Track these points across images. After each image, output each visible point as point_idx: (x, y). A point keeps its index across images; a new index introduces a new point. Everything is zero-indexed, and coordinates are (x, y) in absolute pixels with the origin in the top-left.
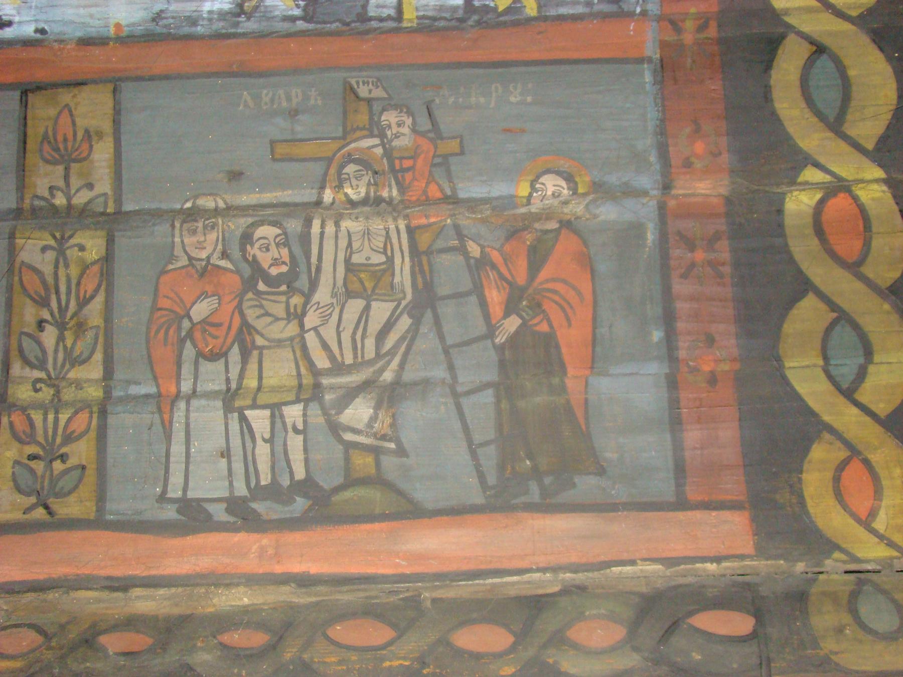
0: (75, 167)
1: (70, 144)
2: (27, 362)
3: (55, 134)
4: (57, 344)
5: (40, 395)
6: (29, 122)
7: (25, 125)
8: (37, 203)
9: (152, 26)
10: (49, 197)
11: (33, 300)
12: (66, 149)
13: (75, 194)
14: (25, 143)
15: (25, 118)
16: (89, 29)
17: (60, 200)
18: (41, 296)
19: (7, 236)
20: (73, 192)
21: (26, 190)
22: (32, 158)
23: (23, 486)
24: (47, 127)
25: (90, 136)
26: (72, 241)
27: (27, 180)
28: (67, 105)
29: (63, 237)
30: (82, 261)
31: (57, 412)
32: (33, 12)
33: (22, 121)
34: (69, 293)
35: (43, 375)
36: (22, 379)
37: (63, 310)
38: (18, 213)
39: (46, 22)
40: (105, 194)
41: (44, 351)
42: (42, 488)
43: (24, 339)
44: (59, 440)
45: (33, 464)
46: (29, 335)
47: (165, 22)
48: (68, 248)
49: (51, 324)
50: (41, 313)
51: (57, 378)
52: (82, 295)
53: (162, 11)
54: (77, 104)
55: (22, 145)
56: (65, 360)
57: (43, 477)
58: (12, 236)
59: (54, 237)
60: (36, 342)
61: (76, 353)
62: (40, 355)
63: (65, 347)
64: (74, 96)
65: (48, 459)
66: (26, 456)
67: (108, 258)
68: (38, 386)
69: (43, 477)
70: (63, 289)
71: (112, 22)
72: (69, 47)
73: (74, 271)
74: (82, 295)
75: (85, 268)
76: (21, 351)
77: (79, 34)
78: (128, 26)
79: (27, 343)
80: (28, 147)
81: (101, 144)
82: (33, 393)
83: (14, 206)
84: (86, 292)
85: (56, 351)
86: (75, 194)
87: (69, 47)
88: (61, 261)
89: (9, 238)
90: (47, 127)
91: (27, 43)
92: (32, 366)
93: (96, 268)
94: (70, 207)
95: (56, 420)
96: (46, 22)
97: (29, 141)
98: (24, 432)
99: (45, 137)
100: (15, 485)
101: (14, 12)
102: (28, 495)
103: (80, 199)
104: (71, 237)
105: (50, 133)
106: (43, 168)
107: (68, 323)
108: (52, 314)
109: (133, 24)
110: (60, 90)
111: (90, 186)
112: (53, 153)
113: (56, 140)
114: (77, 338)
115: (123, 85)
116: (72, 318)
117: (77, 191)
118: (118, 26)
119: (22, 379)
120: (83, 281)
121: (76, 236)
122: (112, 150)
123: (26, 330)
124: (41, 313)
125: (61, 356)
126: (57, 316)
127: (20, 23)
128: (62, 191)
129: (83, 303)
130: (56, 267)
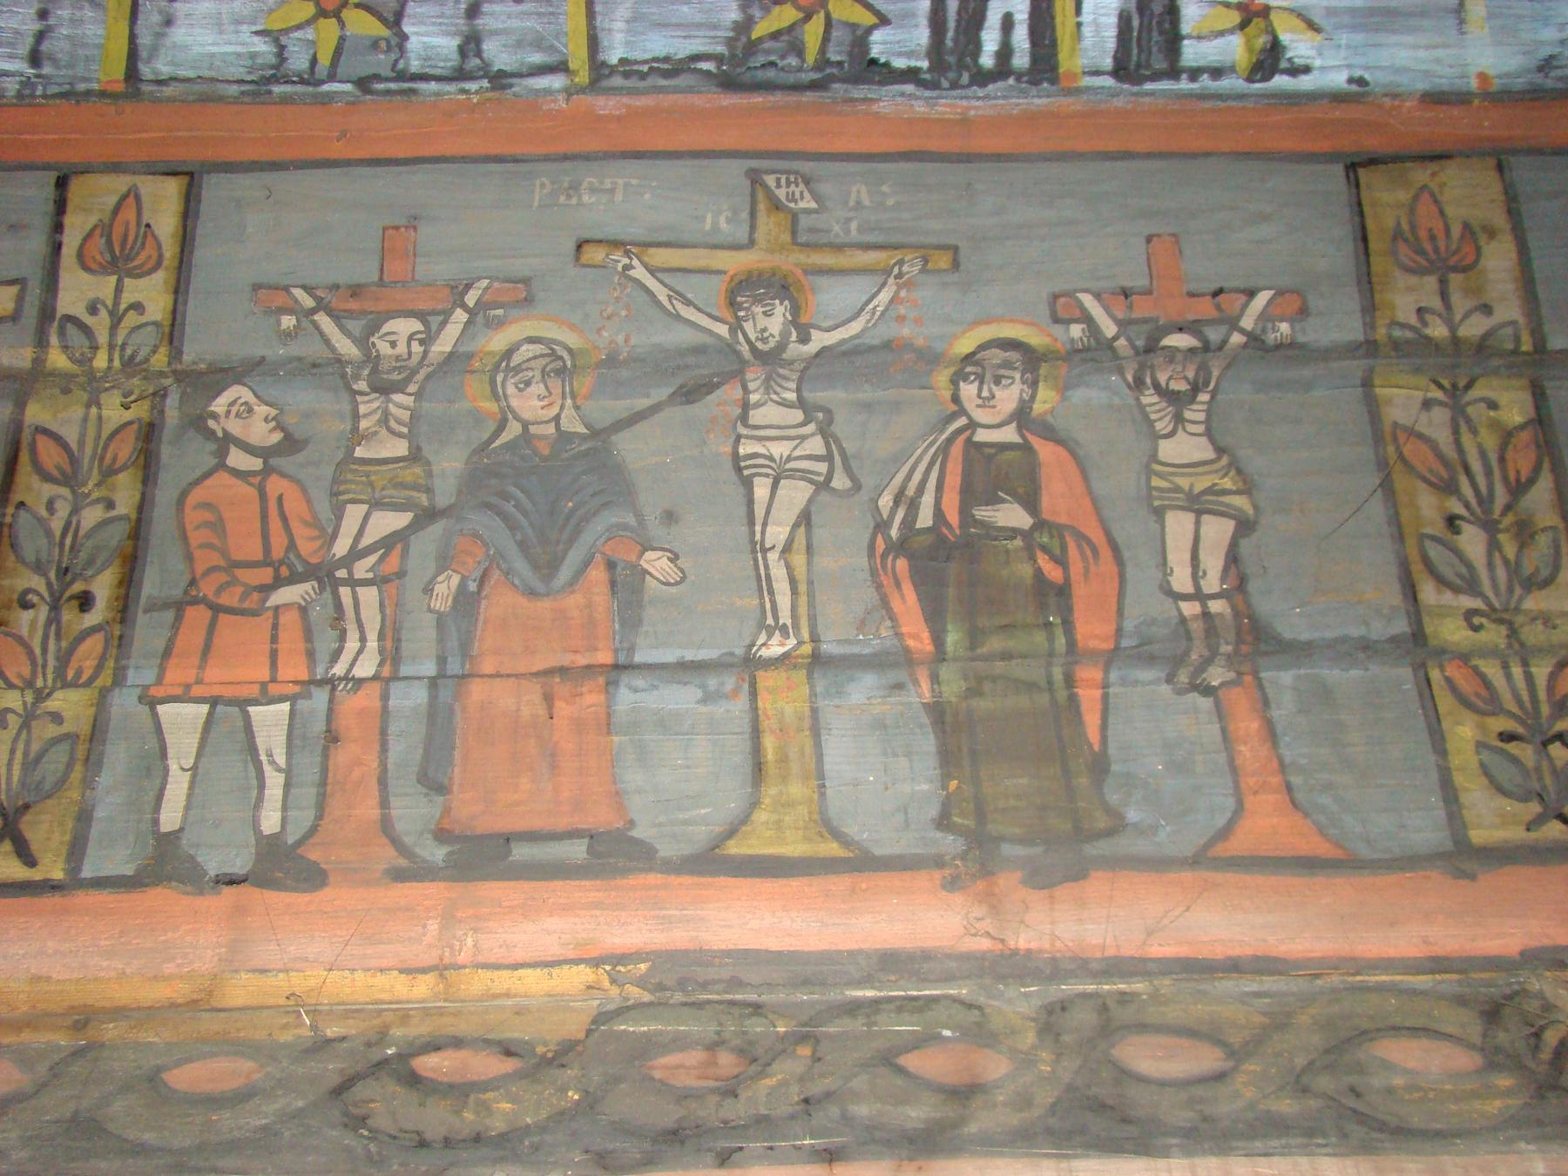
0: (1455, 279)
1: (1442, 244)
2: (1442, 582)
3: (1413, 227)
4: (1490, 555)
5: (1482, 636)
6: (1366, 209)
7: (1361, 214)
8: (1397, 333)
9: (1538, 79)
10: (1418, 325)
11: (1430, 484)
12: (1436, 250)
13: (1462, 320)
14: (1365, 239)
15: (1360, 204)
16: (1437, 80)
17: (1438, 331)
18: (1442, 479)
19: (1358, 382)
20: (1458, 317)
21: (1378, 313)
22: (1378, 263)
23: (1507, 786)
24: (1398, 218)
25: (1473, 233)
26: (1477, 392)
27: (1377, 297)
28: (1424, 188)
29: (1454, 386)
30: (1495, 425)
31: (1525, 664)
32: (1343, 53)
33: (1356, 209)
34: (1488, 473)
35: (1477, 604)
36: (1443, 612)
37: (1485, 501)
38: (1370, 348)
39: (1367, 68)
40: (1513, 323)
41: (1469, 565)
42: (1544, 787)
43: (1428, 543)
44: (1545, 710)
45: (1512, 748)
46: (1433, 538)
47: (1559, 72)
48: (1468, 404)
49: (1469, 522)
50: (1447, 504)
51: (1506, 610)
52: (1512, 476)
53: (1552, 57)
54: (1442, 185)
55: (1361, 244)
56: (1510, 581)
57: (1538, 769)
58: (1367, 384)
59: (1440, 386)
60: (1451, 550)
61: (1527, 569)
62: (1464, 570)
63: (1506, 562)
64: (1433, 175)
65: (1538, 739)
66: (1494, 735)
67: (1541, 420)
68: (1476, 620)
69: (1538, 769)
70: (1476, 466)
71: (1473, 70)
72: (1408, 104)
73: (1490, 441)
74: (1512, 476)
75: (1507, 436)
76: (1426, 561)
77: (1421, 86)
78: (1499, 77)
79: (1434, 551)
80: (1372, 245)
81: (1494, 244)
82: (1470, 633)
83: (1359, 336)
84: (1518, 472)
85: (1490, 565)
86: (1462, 320)
87: (1408, 104)
88: (1462, 423)
89: (1363, 385)
90: (1398, 218)
91: (1337, 98)
92: (1457, 590)
93: (1525, 436)
94: (1455, 341)
95: (1529, 678)
96: (1367, 68)
97: (1371, 237)
98: (1477, 695)
99: (1397, 235)
100: (1491, 782)
101: (1313, 53)
102: (1525, 800)
103: (1473, 328)
104: (1469, 386)
105: (1405, 226)
106: (1402, 280)
107: (1498, 522)
108: (1467, 506)
109: (1507, 75)
110: (1408, 165)
111: (1487, 309)
112: (1418, 258)
113: (1417, 239)
114: (1522, 547)
115: (1512, 159)
116: (1503, 514)
117: (1467, 315)
118: (1482, 77)
119: (1443, 612)
120: (1509, 455)
121: (1478, 384)
122: (1514, 255)
123: (1428, 531)
124: (1447, 504)
125: (1501, 573)
126: (1478, 510)
127: (1323, 68)
128: (1440, 315)
129: (1518, 489)
130: (1456, 432)
